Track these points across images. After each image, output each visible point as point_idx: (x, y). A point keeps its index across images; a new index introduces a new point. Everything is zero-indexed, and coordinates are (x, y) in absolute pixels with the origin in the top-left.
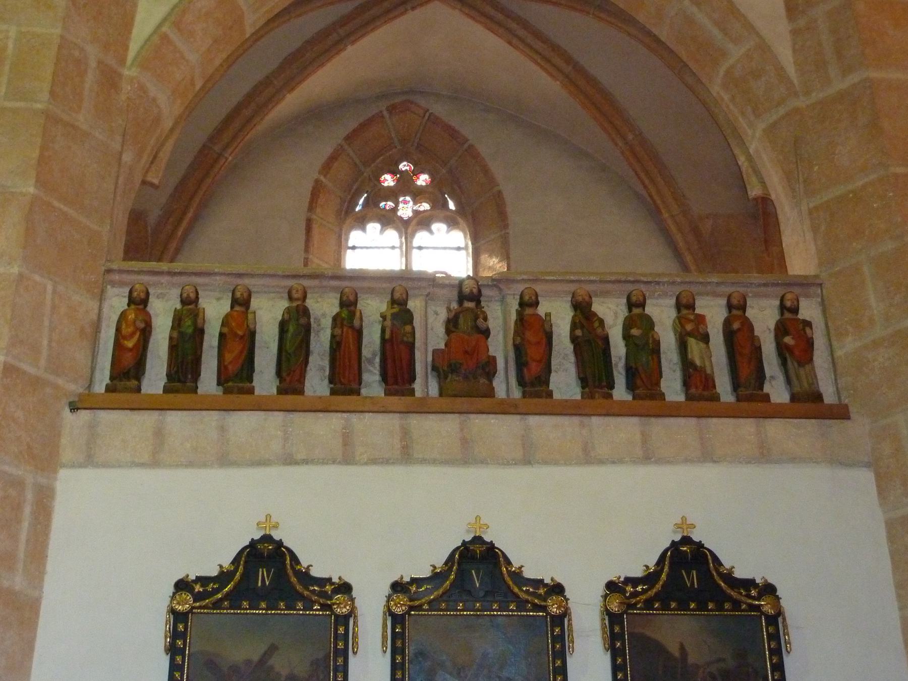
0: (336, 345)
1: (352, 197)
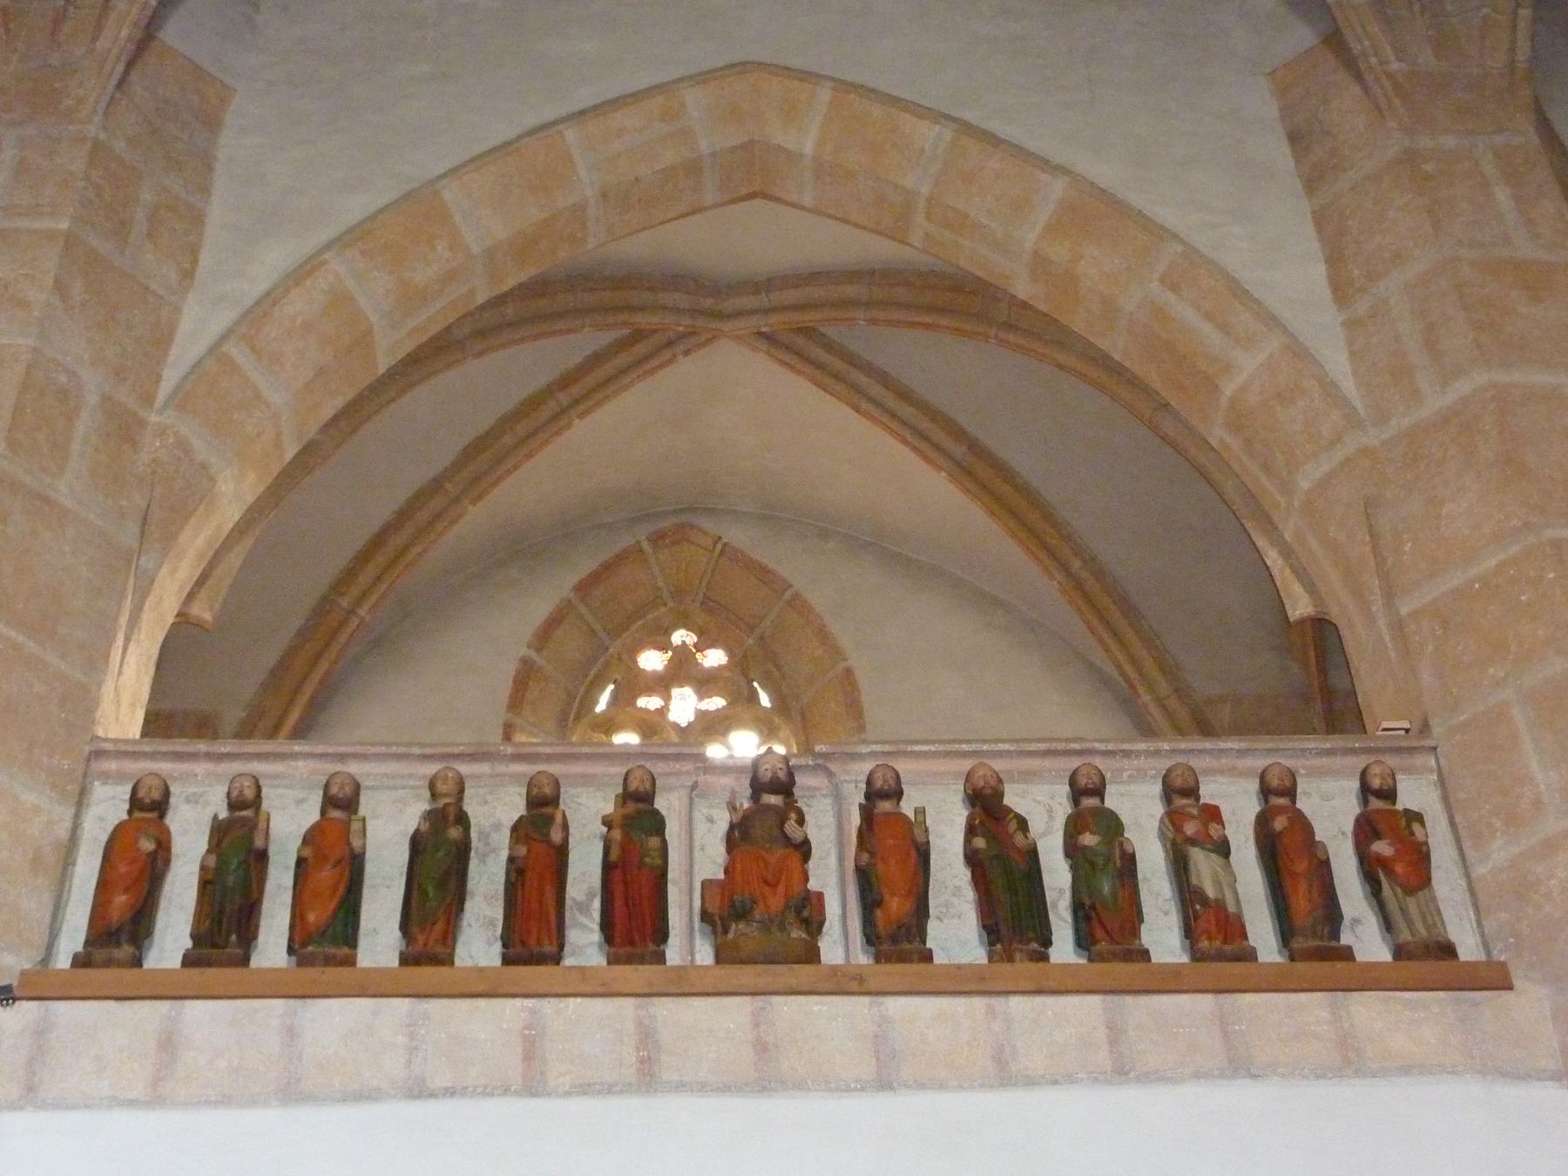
0: (517, 873)
1: (588, 691)
